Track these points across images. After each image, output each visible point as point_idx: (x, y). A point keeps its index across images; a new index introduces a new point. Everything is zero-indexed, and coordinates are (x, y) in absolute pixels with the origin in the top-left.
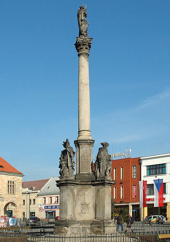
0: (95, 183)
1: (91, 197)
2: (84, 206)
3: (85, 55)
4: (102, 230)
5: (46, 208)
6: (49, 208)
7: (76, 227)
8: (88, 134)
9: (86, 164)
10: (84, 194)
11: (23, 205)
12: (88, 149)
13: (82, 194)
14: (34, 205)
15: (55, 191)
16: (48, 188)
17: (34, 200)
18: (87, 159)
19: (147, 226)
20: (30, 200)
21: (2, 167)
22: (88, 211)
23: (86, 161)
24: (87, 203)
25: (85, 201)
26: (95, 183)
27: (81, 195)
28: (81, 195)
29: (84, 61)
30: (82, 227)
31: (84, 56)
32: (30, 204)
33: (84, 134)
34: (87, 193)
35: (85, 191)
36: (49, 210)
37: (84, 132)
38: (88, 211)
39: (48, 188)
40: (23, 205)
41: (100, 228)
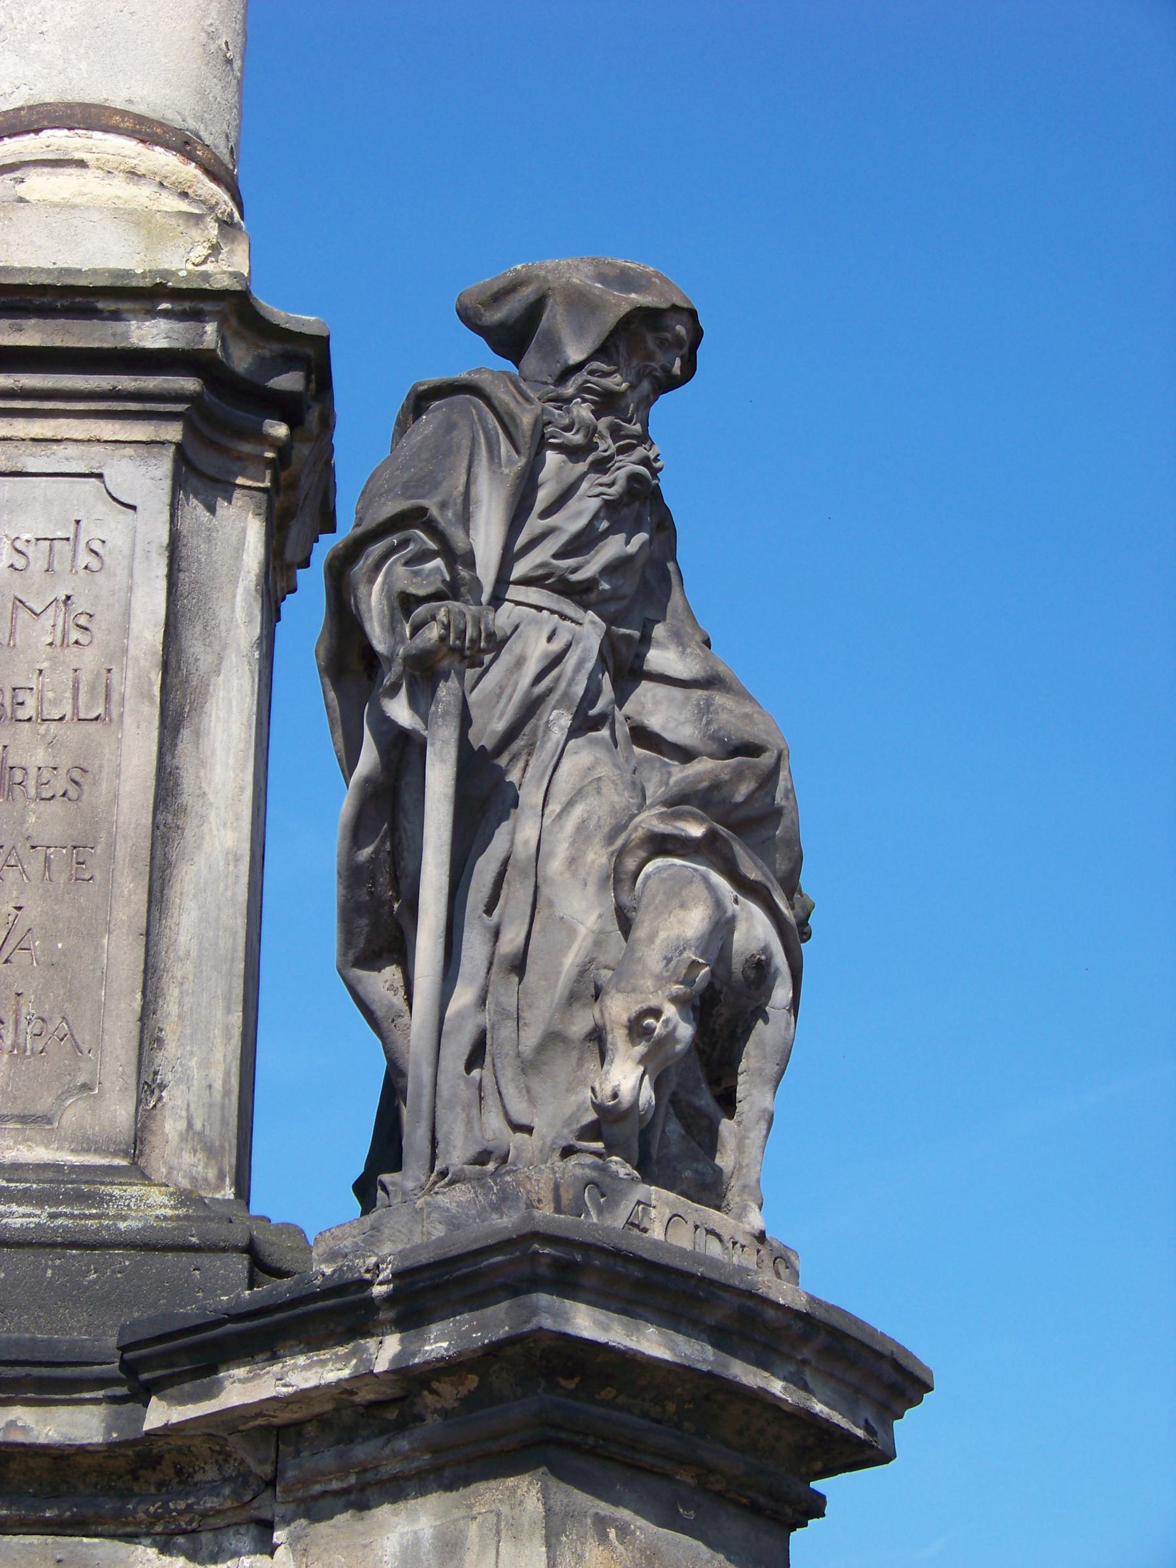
26: (242, 1388)
37: (55, 140)
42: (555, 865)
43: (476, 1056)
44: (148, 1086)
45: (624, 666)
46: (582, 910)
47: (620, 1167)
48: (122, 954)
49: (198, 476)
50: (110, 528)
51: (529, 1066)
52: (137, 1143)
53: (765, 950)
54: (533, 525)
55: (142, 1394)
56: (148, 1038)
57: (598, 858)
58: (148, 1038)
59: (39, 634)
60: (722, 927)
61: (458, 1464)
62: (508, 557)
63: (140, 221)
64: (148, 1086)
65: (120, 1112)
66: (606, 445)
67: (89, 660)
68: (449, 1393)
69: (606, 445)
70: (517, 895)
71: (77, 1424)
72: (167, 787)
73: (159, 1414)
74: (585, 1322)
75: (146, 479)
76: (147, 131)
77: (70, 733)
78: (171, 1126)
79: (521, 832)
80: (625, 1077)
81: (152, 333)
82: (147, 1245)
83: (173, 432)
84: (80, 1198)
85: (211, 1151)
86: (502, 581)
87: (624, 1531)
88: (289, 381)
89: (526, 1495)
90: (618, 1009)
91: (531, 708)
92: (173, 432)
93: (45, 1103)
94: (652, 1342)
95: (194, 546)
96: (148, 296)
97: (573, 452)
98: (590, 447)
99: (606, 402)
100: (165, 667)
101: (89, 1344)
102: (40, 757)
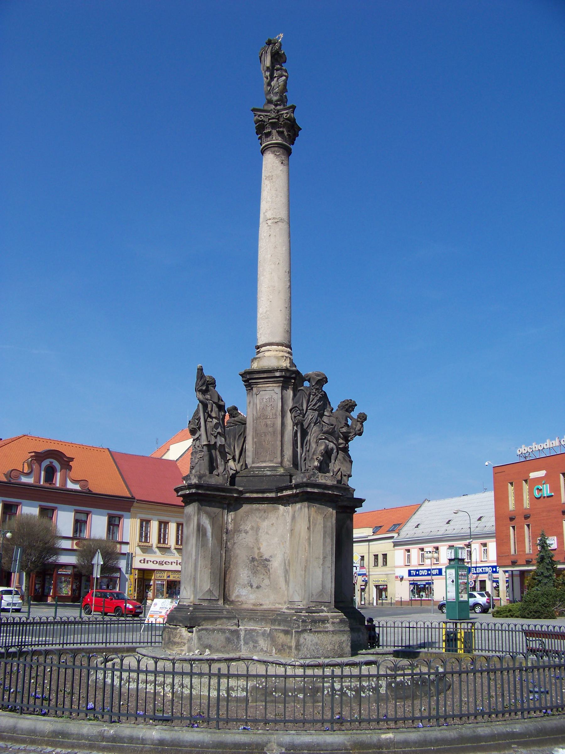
0: (285, 493)
1: (276, 539)
2: (256, 563)
3: (276, 149)
4: (293, 644)
5: (413, 576)
6: (422, 575)
7: (223, 631)
8: (282, 354)
9: (269, 438)
10: (258, 528)
11: (375, 566)
12: (275, 396)
13: (252, 528)
14: (384, 568)
15: (432, 534)
16: (417, 527)
17: (385, 556)
18: (274, 424)
19: (417, 628)
20: (376, 556)
21: (1, 439)
22: (267, 582)
23: (270, 429)
24: (266, 556)
25: (259, 549)
26: (285, 493)
27: (246, 532)
28: (246, 532)
29: (272, 166)
30: (246, 631)
31: (273, 152)
32: (376, 565)
33: (267, 354)
34: (265, 524)
35: (260, 518)
36: (422, 580)
37: (268, 347)
38: (267, 582)
39: (417, 527)
40: (375, 566)
41: (289, 636)
42: (311, 441)
43: (305, 460)
44: (282, 456)
45: (321, 415)
46: (314, 445)
47: (316, 472)
48: (279, 443)
49: (284, 388)
50: (275, 396)
51: (310, 461)
52: (281, 463)
53: (332, 448)
54: (310, 404)
55: (278, 492)
56: (282, 451)
57: (315, 440)
58: (282, 451)
59: (269, 409)
60: (327, 446)
61: (302, 501)
62: (307, 407)
63: (277, 358)
64: (282, 456)
65: (279, 460)
66: (317, 394)
67: (274, 411)
68: (301, 494)
69: (317, 394)
70: (308, 444)
71: (272, 495)
72: (283, 424)
73: (279, 495)
74: (309, 490)
75: (278, 390)
76: (278, 344)
77: (272, 420)
78: (286, 460)
79: (308, 438)
80: (316, 463)
81: (278, 374)
82: (280, 475)
83: (281, 384)
84: (275, 470)
85: (290, 462)
86: (307, 410)
87: (316, 506)
88: (294, 376)
89: (306, 504)
90: (315, 457)
91: (310, 424)
92: (281, 384)
93: (272, 459)
94: (316, 490)
95: (285, 396)
96: (277, 370)
97: (313, 395)
98: (315, 394)
99: (317, 389)
100: (282, 412)
101: (45, 747)
102: (270, 423)
